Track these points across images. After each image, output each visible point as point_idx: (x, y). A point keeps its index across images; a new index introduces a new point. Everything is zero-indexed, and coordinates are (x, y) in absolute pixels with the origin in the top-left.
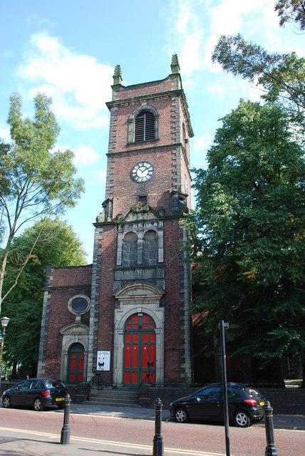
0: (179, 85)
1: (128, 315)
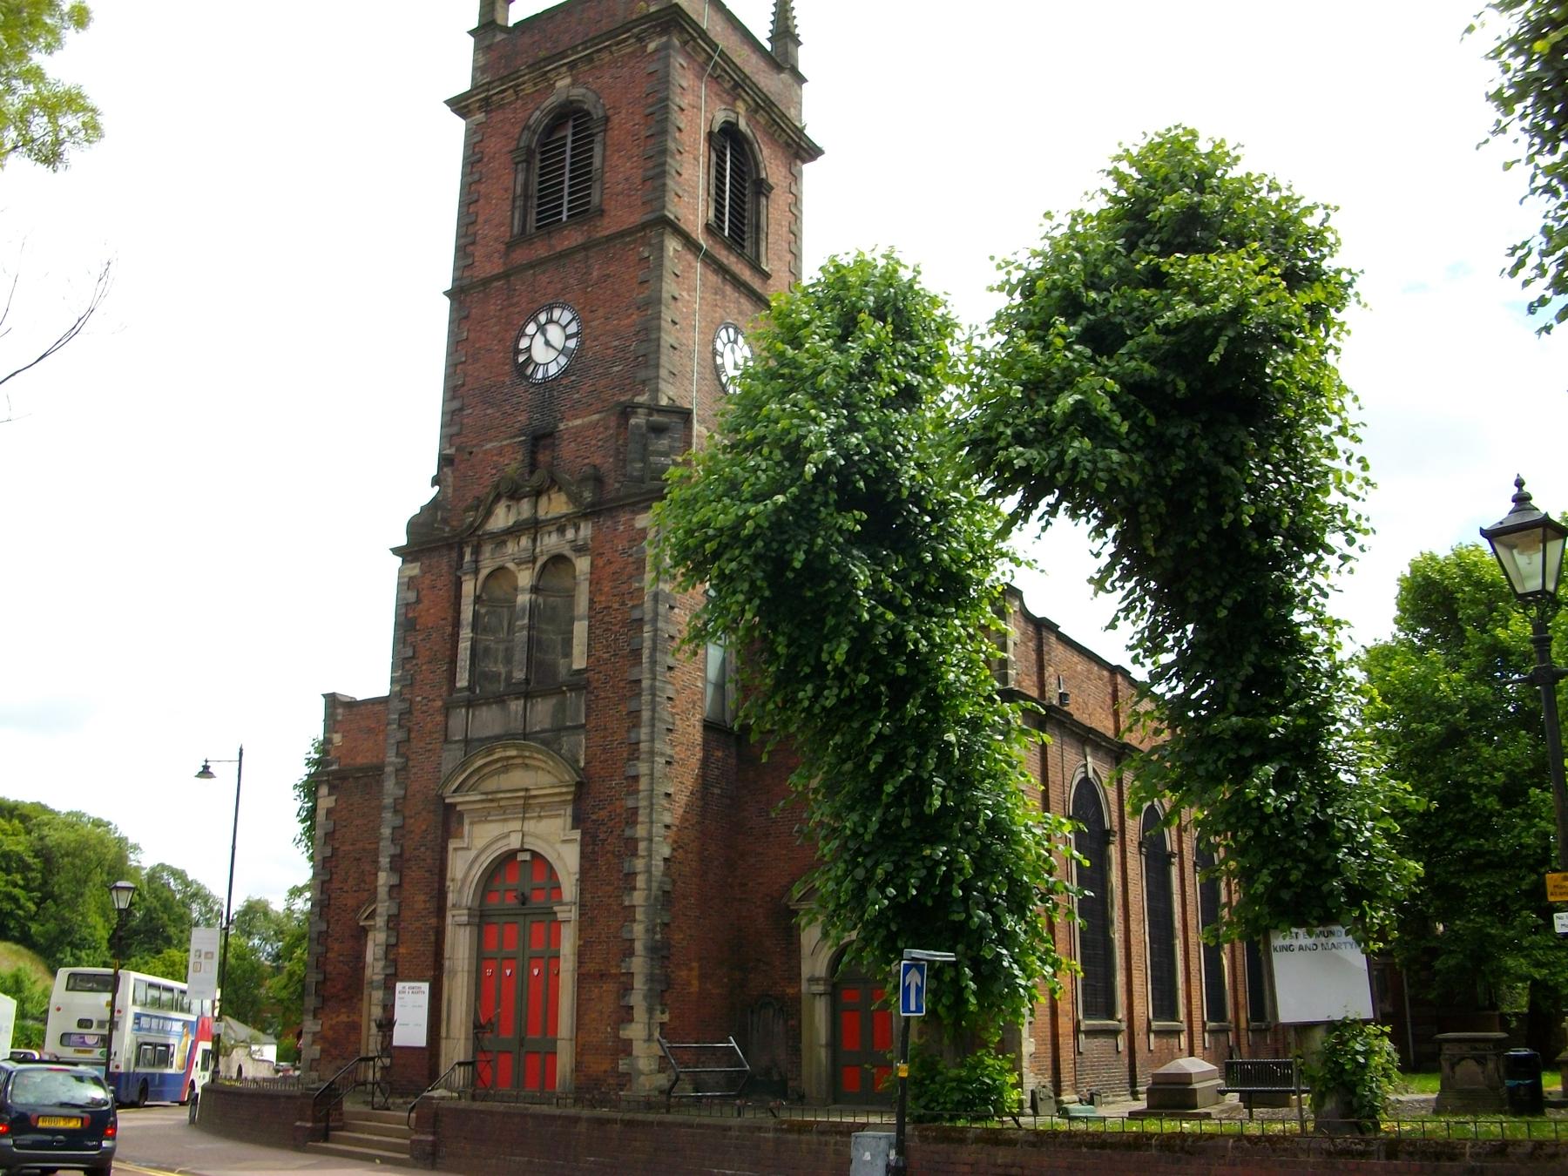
1: (486, 860)
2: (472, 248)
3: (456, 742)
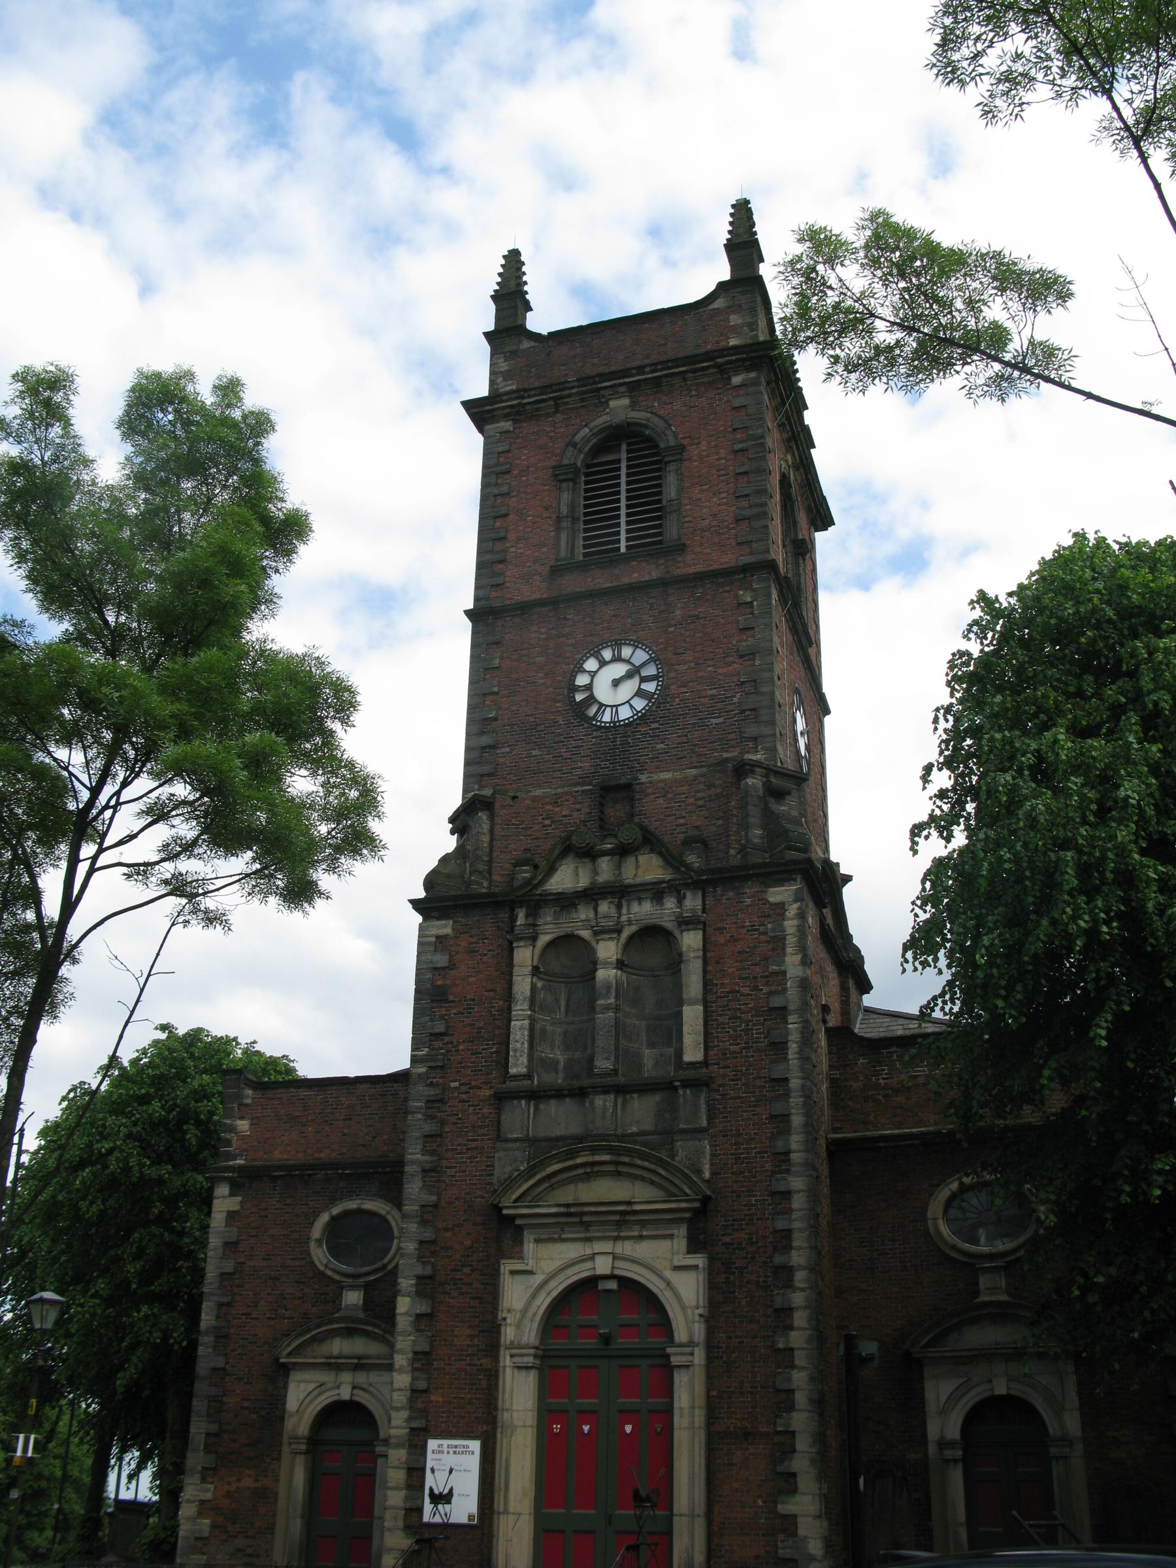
0: (762, 323)
1: (557, 1286)
2: (501, 566)
3: (516, 1140)
